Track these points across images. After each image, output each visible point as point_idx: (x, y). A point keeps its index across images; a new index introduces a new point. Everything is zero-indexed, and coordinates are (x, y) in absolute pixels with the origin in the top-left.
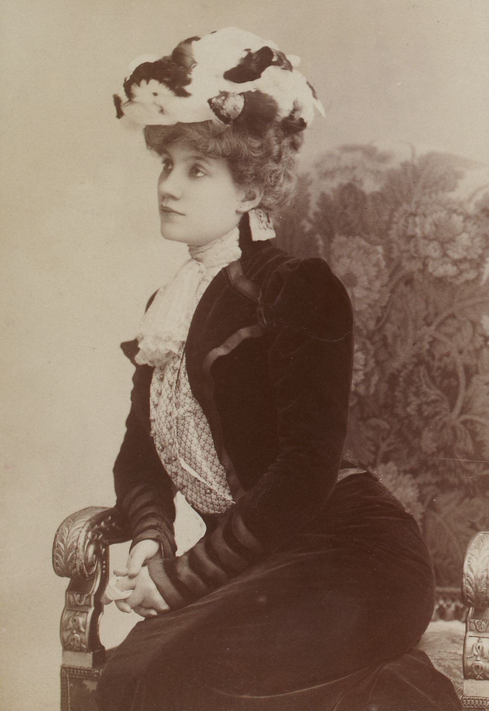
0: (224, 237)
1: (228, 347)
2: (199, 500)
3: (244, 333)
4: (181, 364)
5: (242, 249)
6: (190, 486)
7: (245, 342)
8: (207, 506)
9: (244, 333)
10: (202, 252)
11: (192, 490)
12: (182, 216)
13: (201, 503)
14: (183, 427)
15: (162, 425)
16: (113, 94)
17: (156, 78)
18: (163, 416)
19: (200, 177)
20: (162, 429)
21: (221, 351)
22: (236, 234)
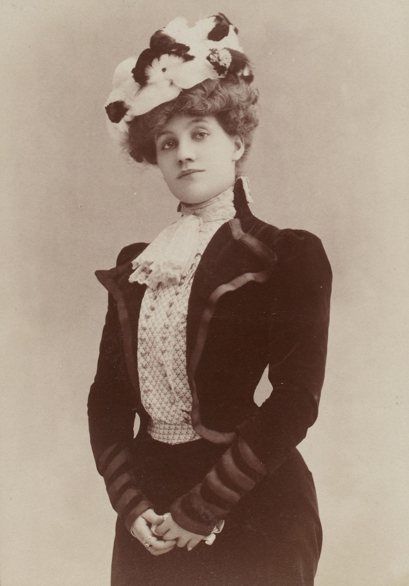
0: (220, 196)
1: (234, 285)
2: (158, 405)
3: (249, 277)
4: (185, 291)
5: (236, 209)
6: (154, 392)
7: (250, 284)
8: (162, 413)
9: (249, 277)
10: (201, 209)
11: (155, 395)
12: (202, 173)
13: (159, 409)
14: (149, 349)
15: (155, 334)
16: (167, 68)
17: (165, 53)
18: (159, 327)
19: (167, 149)
20: (154, 338)
21: (225, 288)
22: (230, 195)
